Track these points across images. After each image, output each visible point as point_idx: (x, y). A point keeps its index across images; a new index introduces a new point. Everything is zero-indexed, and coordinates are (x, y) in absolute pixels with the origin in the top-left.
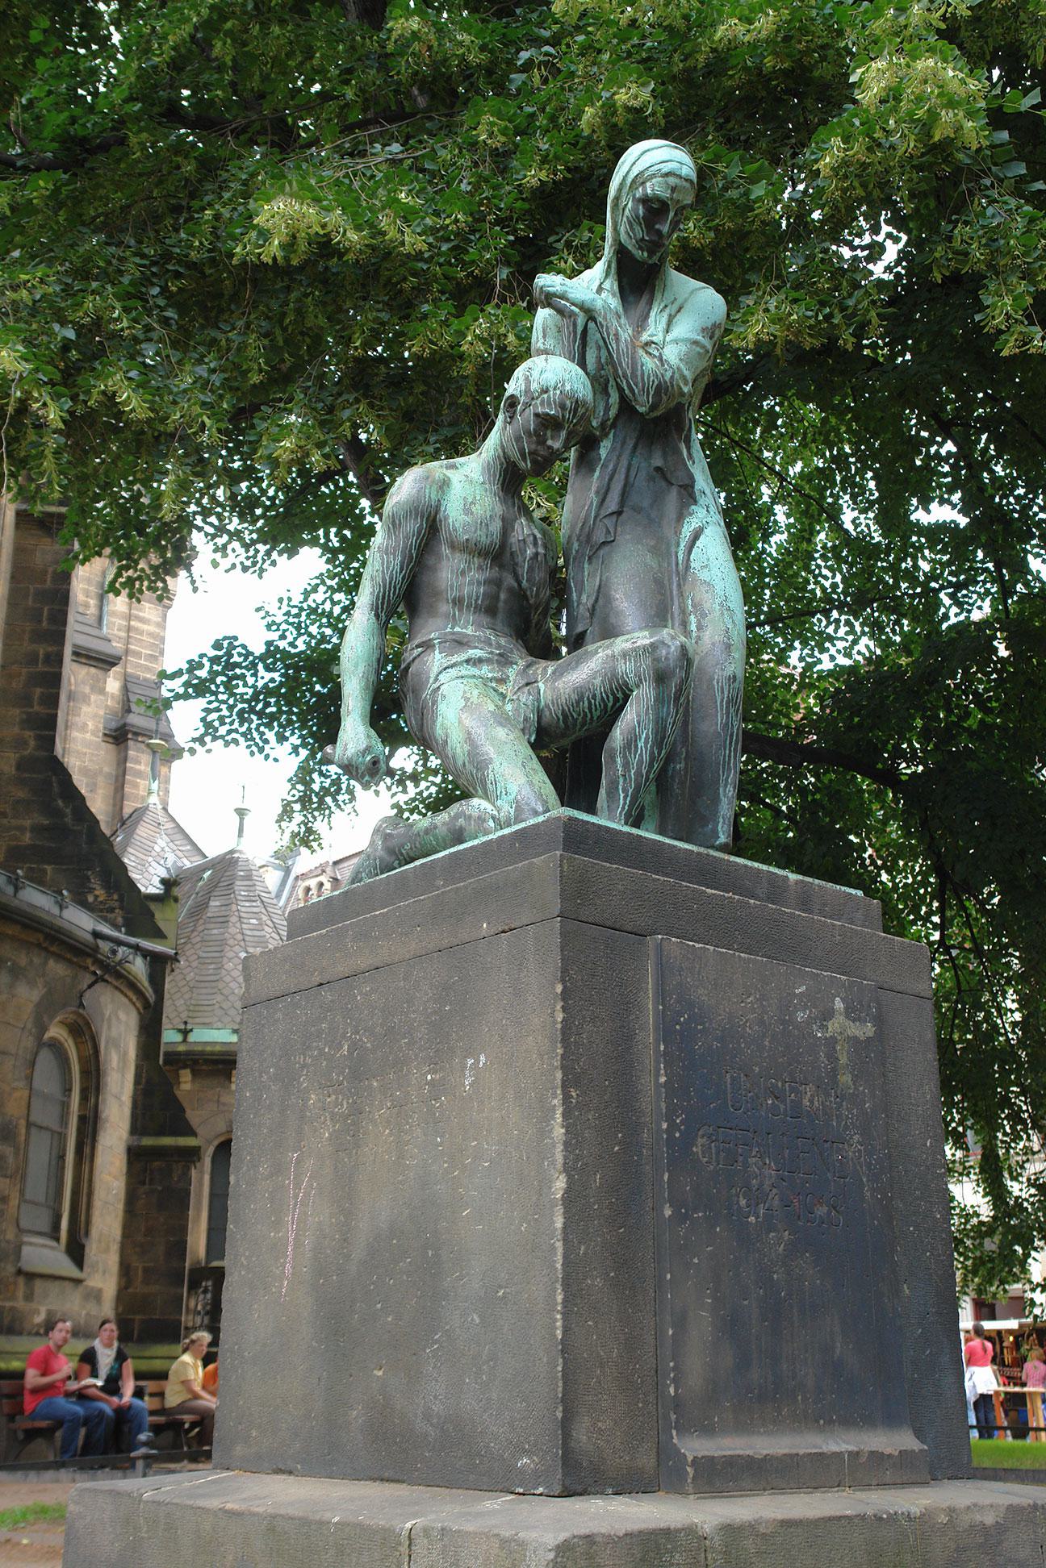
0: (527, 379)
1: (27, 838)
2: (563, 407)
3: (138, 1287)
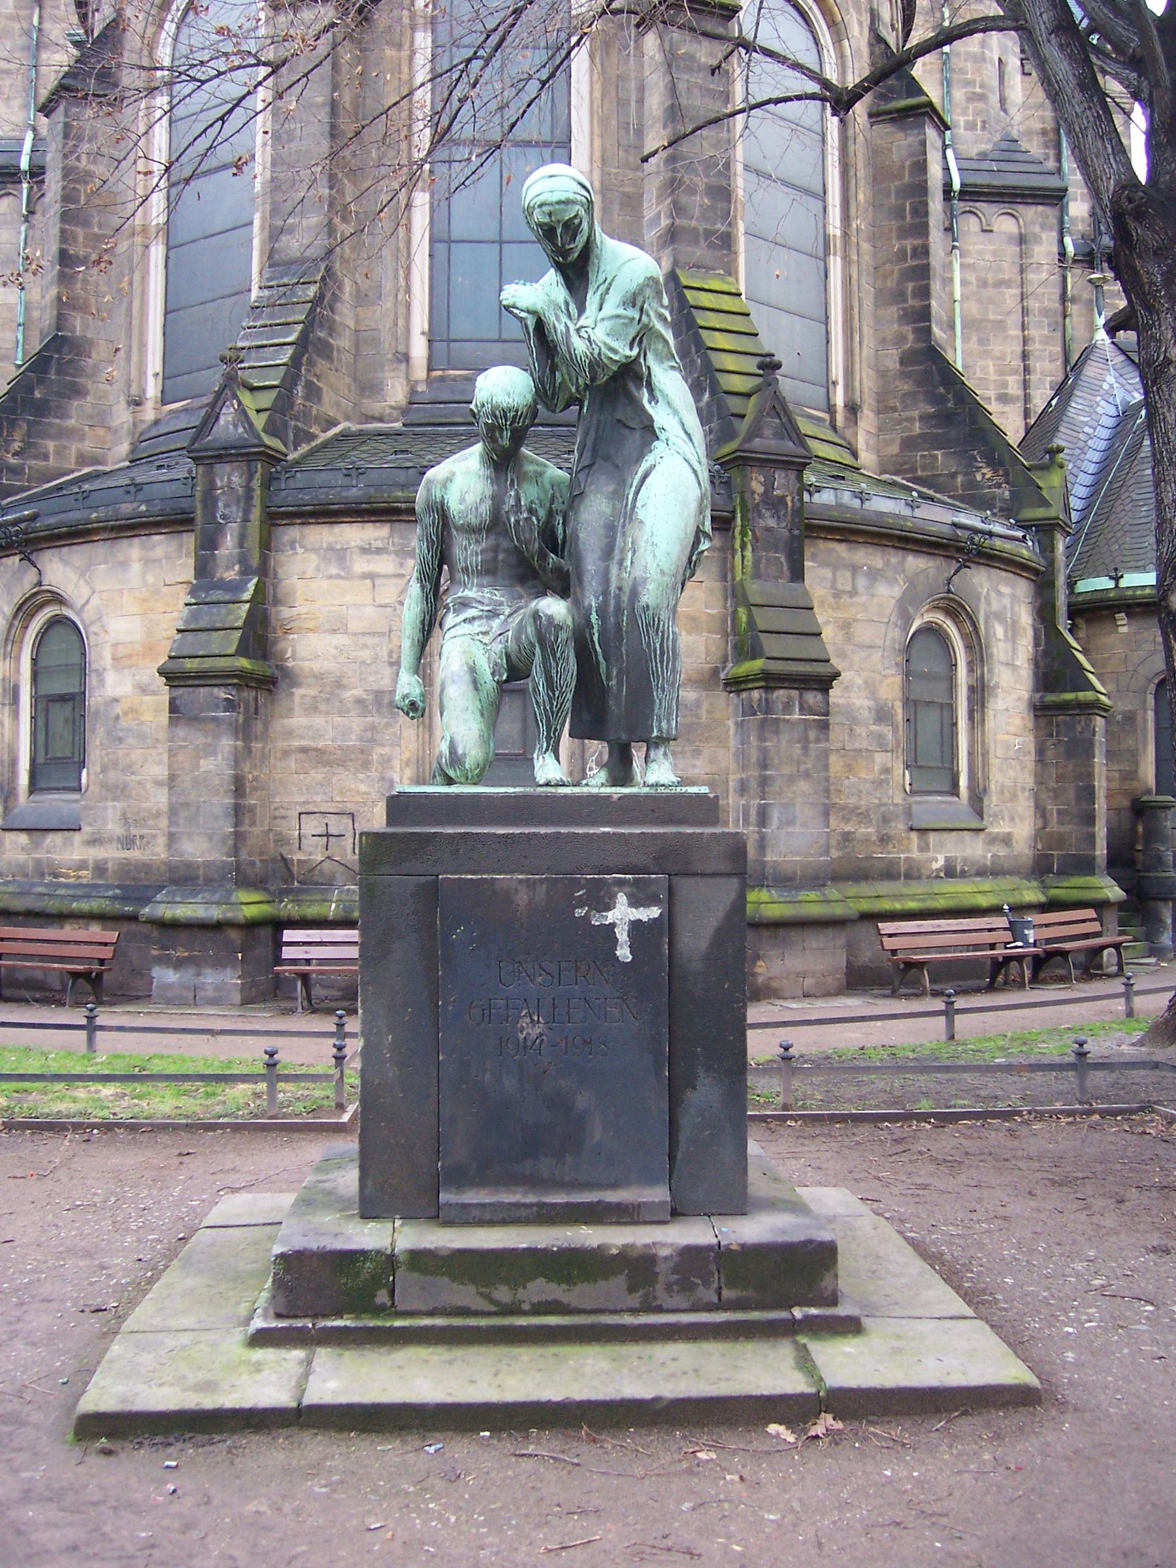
1: (917, 428)
3: (1054, 826)
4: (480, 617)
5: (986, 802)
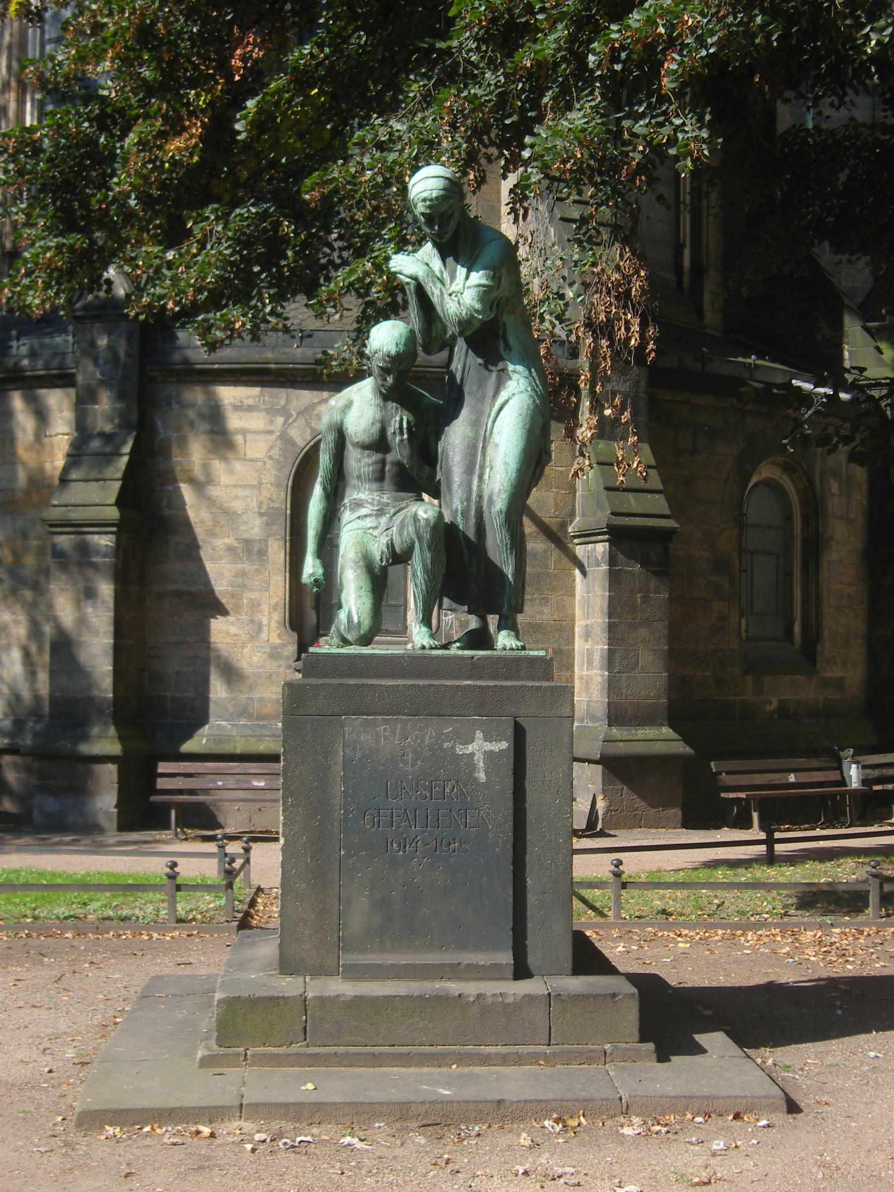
2: (384, 361)
4: (370, 515)
5: (819, 648)
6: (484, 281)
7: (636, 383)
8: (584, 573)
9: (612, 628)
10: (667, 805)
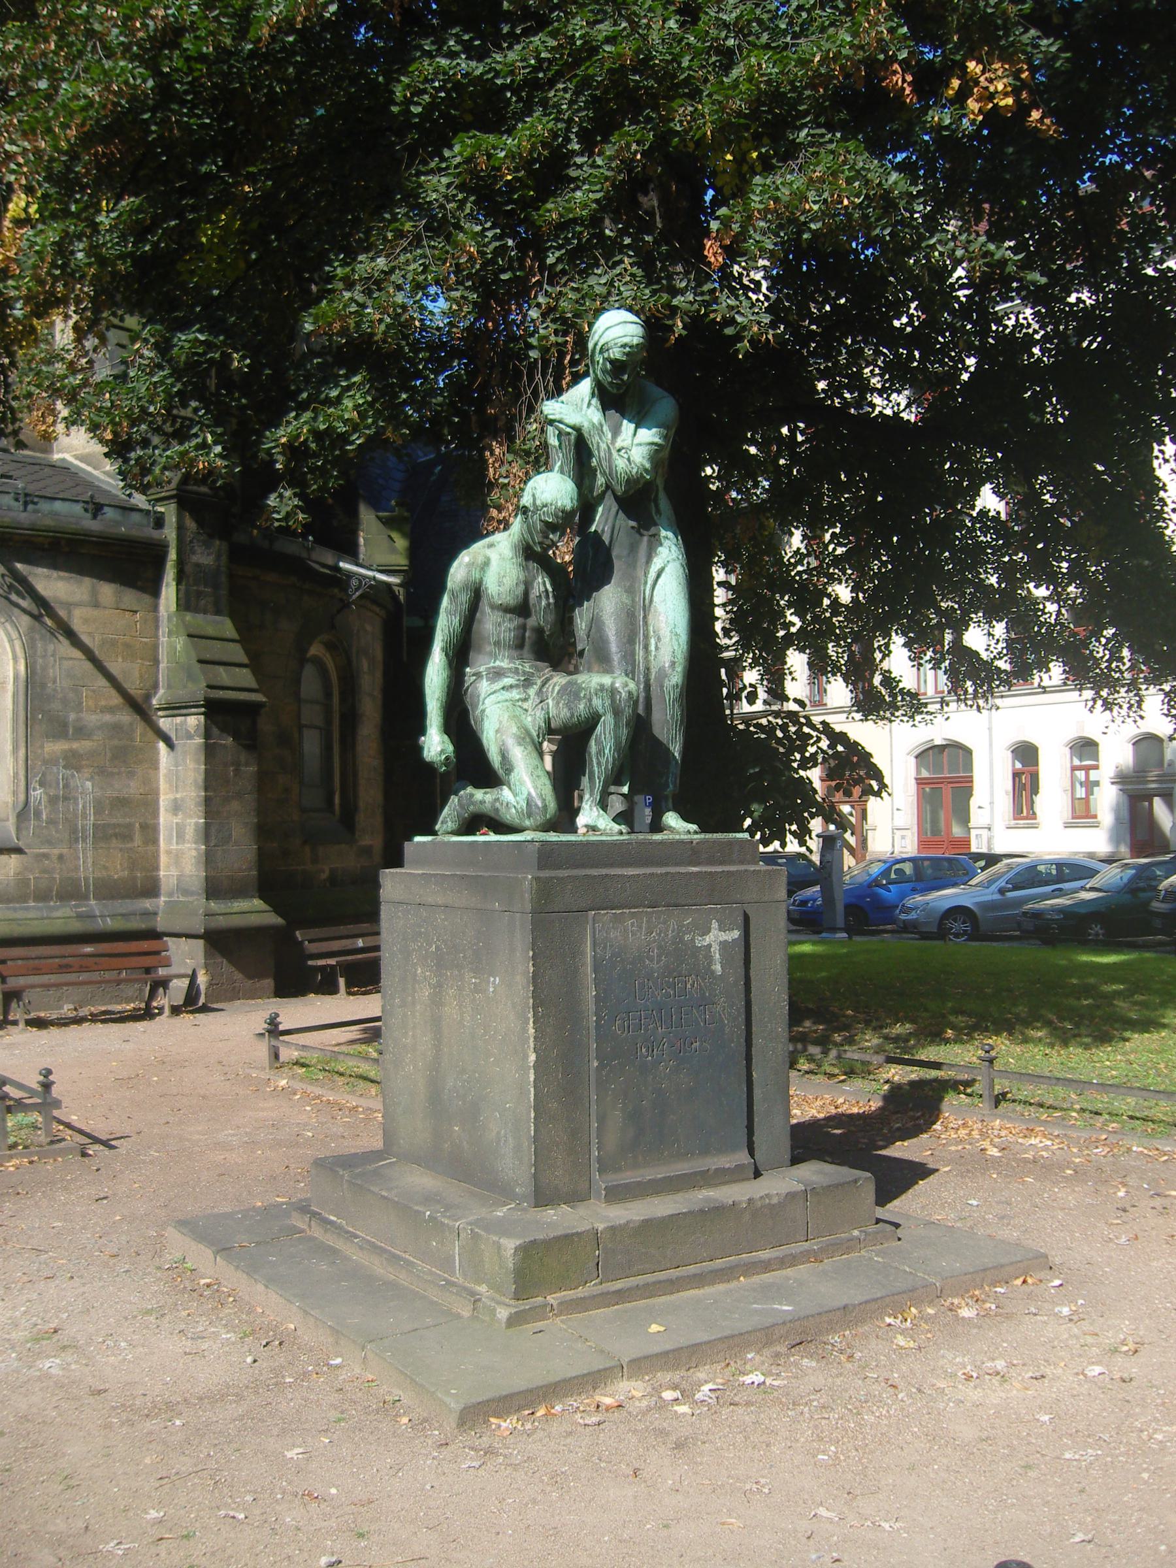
0: (534, 495)
2: (557, 516)
6: (657, 440)
7: (218, 557)
8: (170, 745)
9: (208, 801)
10: (261, 976)
